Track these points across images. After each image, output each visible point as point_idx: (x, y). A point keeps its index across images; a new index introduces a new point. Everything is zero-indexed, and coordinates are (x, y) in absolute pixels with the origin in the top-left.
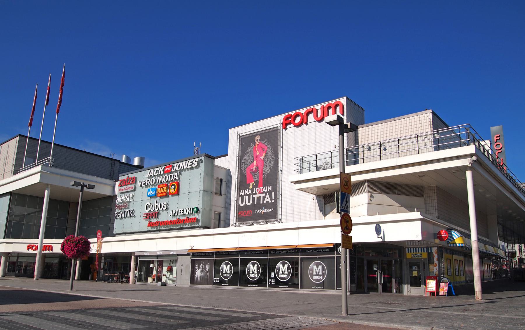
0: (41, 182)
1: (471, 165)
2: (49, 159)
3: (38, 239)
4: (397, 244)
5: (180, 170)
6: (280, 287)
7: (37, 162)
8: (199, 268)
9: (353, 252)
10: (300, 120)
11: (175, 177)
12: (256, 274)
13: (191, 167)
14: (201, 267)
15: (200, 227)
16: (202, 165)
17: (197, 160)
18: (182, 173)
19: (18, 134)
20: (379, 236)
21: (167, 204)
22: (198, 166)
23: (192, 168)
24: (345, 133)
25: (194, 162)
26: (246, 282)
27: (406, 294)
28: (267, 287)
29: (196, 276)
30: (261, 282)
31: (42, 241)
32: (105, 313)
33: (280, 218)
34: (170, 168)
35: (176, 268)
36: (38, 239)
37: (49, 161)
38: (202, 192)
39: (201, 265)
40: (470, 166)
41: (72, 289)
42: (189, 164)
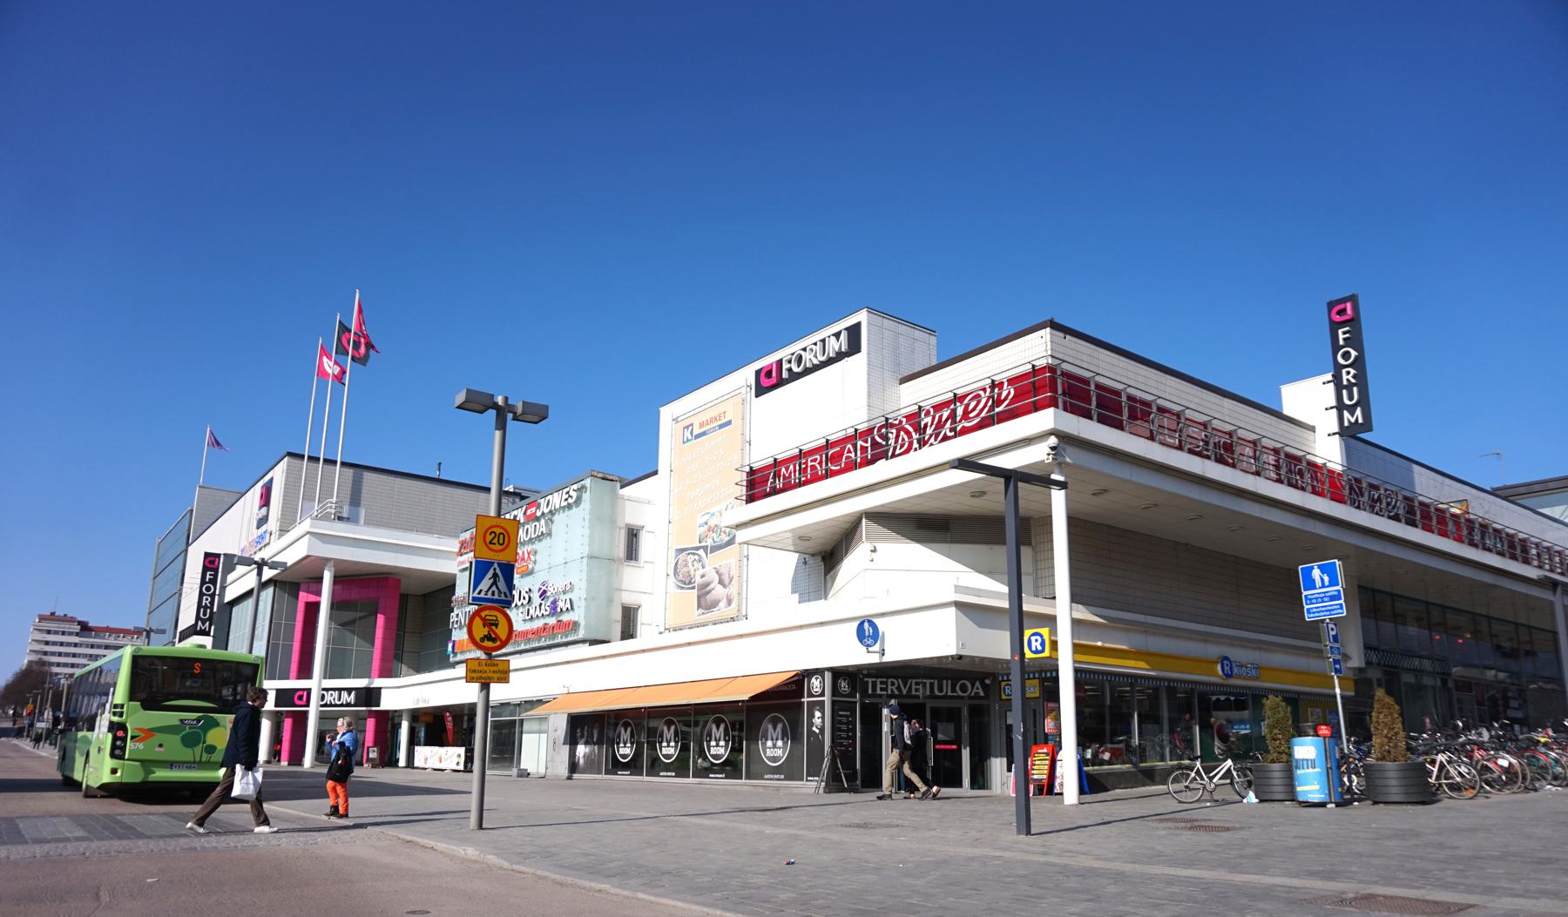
0: (310, 554)
1: (1051, 460)
2: (332, 503)
3: (311, 678)
4: (911, 664)
5: (551, 511)
6: (663, 776)
7: (316, 508)
8: (582, 736)
9: (818, 690)
10: (464, 397)
11: (541, 530)
12: (780, 748)
13: (566, 503)
14: (586, 733)
15: (583, 641)
16: (586, 496)
17: (575, 487)
18: (556, 518)
19: (284, 453)
20: (870, 649)
21: (530, 590)
22: (578, 501)
23: (569, 506)
24: (1333, 375)
25: (572, 493)
26: (655, 766)
27: (999, 792)
28: (742, 778)
29: (577, 754)
30: (680, 767)
31: (320, 683)
32: (1239, 875)
33: (744, 614)
34: (533, 509)
35: (546, 735)
36: (311, 678)
37: (331, 507)
38: (585, 560)
39: (586, 728)
40: (1048, 461)
41: (470, 793)
42: (565, 496)
